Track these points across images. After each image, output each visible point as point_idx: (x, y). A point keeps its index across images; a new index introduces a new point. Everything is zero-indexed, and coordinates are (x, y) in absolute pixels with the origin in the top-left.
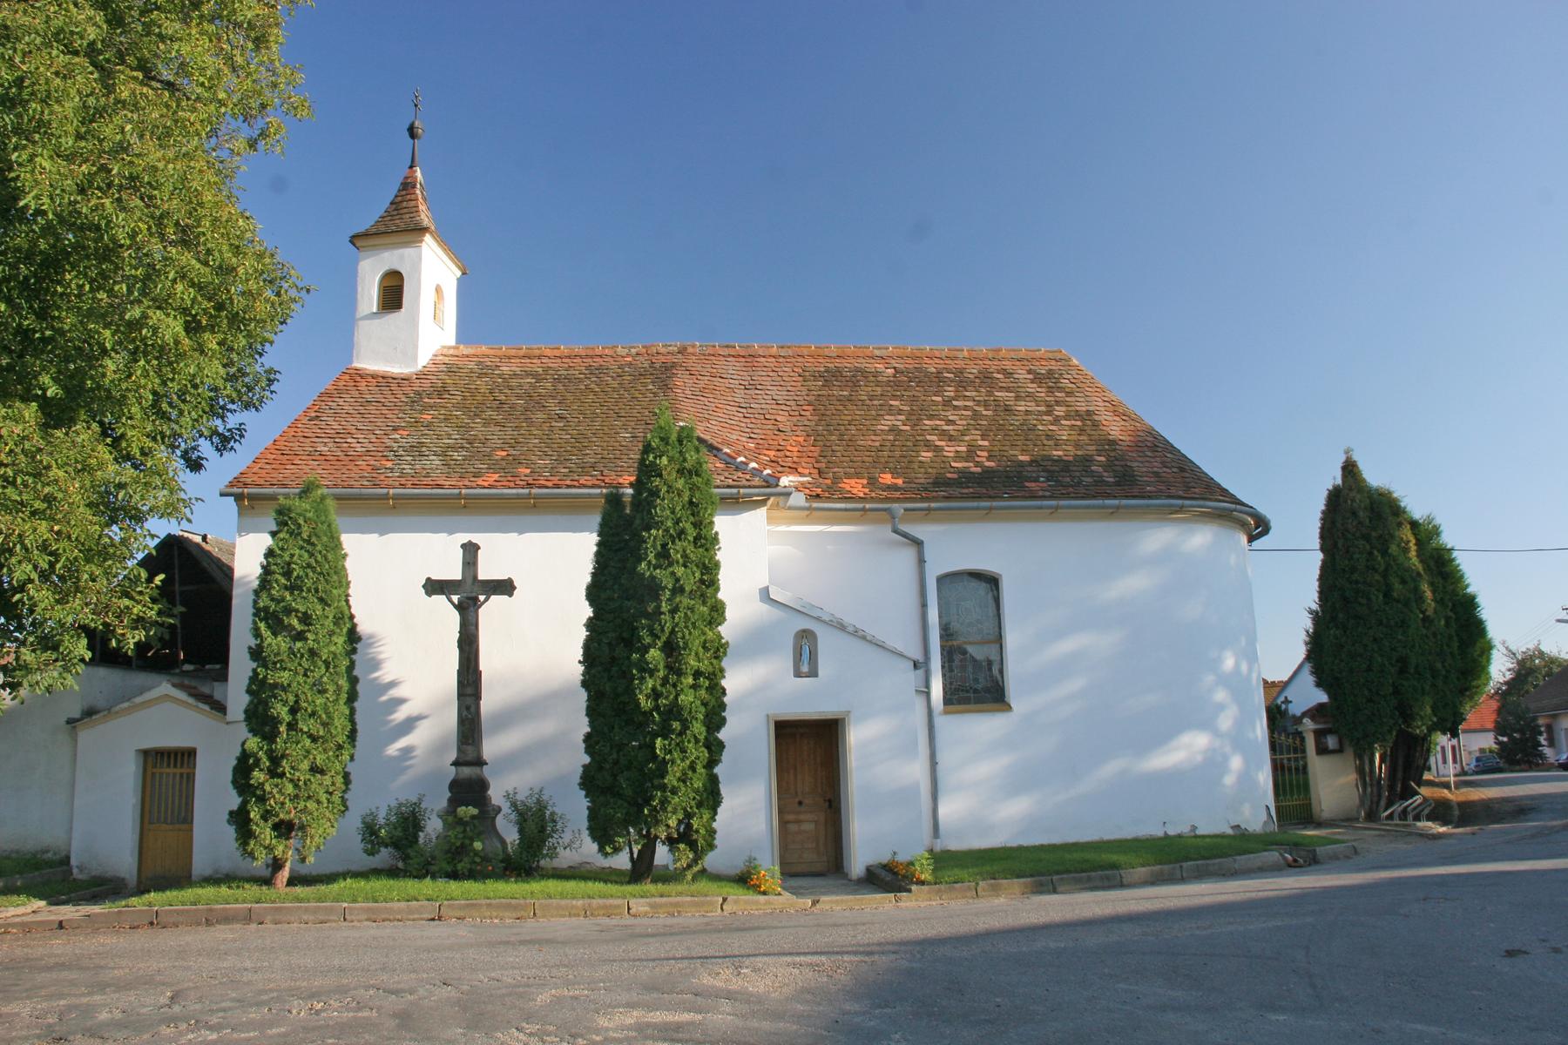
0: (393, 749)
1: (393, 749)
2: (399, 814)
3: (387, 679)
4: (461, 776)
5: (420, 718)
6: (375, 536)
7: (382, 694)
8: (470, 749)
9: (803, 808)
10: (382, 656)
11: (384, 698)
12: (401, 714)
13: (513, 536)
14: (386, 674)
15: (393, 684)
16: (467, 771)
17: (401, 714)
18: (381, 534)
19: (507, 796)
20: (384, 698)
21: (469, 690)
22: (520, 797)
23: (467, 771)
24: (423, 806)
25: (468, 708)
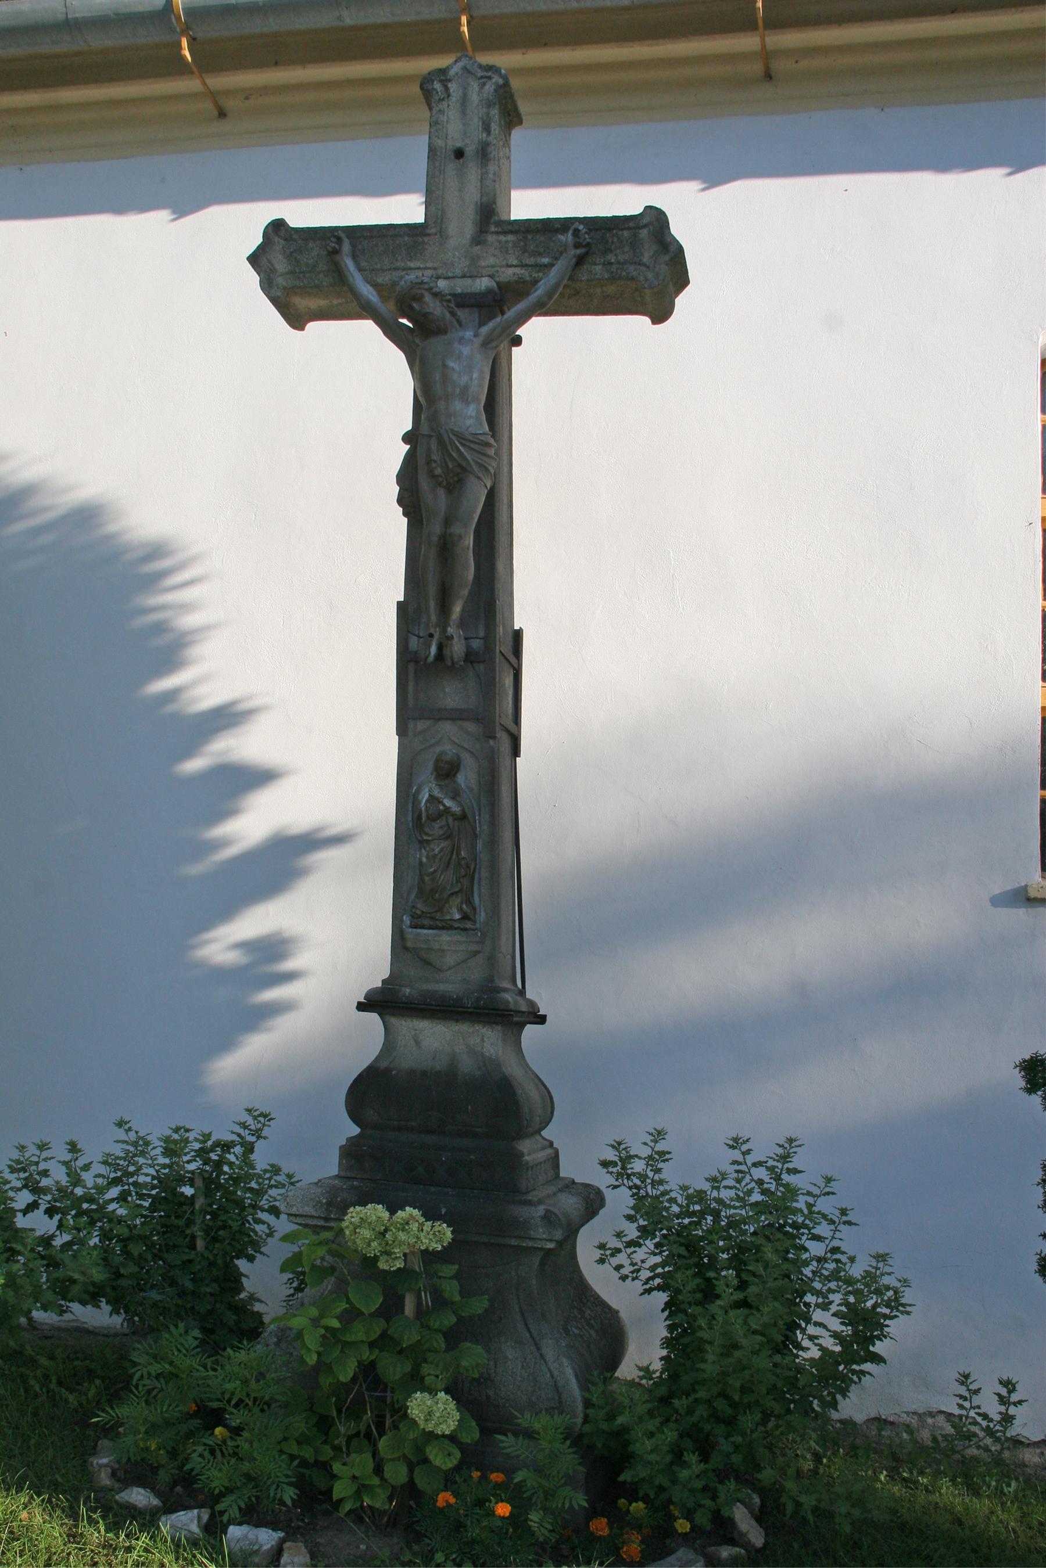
0: (223, 943)
1: (223, 943)
2: (167, 1194)
3: (208, 697)
4: (408, 1059)
5: (311, 842)
6: (161, 217)
7: (190, 750)
8: (450, 946)
9: (491, 271)
10: (189, 621)
11: (195, 765)
12: (253, 823)
13: (990, 181)
14: (206, 678)
15: (227, 717)
16: (433, 1040)
17: (253, 823)
18: (181, 211)
19: (619, 1165)
20: (195, 765)
21: (452, 694)
22: (676, 1177)
23: (433, 1040)
24: (261, 1159)
25: (447, 771)
